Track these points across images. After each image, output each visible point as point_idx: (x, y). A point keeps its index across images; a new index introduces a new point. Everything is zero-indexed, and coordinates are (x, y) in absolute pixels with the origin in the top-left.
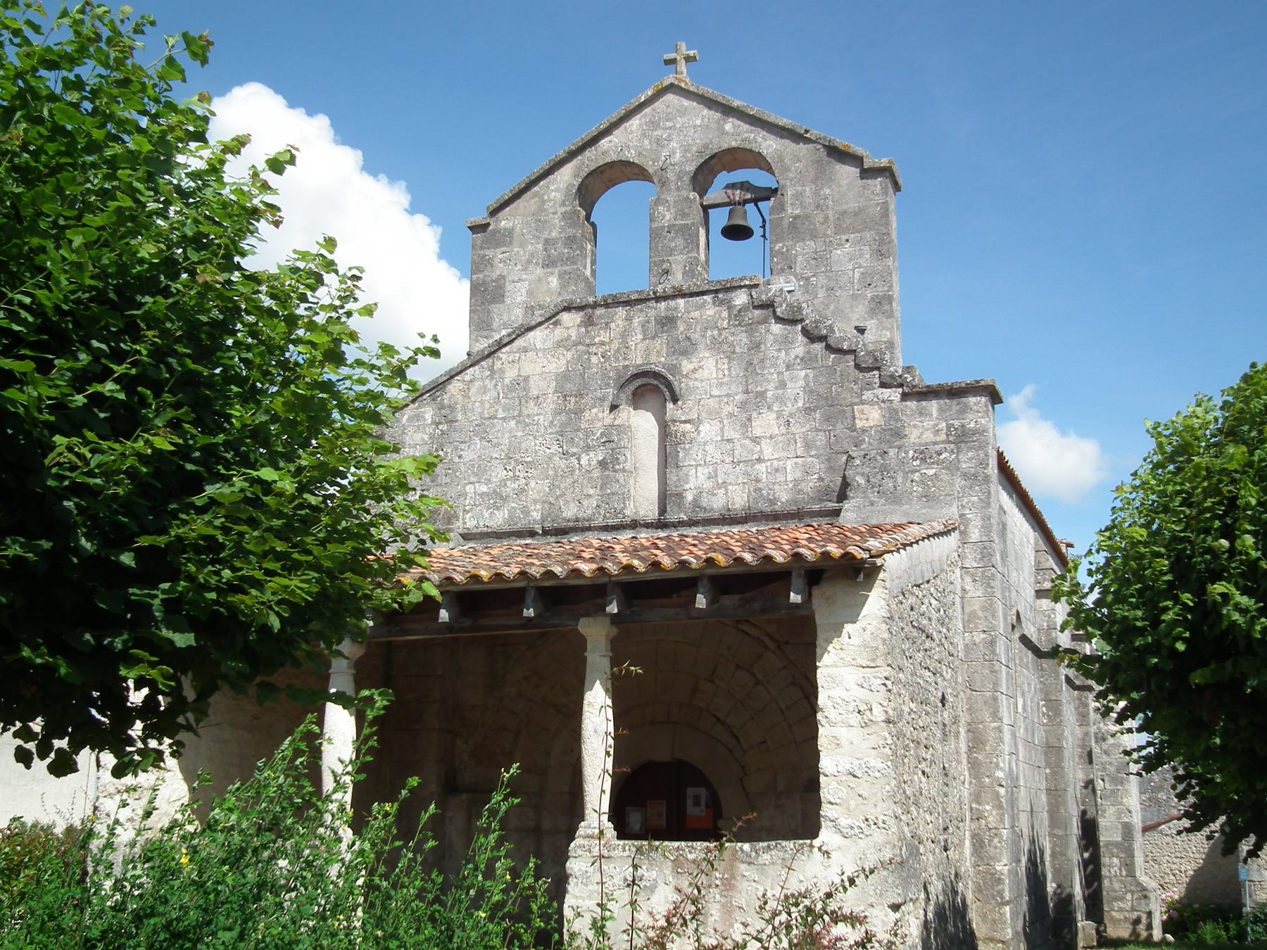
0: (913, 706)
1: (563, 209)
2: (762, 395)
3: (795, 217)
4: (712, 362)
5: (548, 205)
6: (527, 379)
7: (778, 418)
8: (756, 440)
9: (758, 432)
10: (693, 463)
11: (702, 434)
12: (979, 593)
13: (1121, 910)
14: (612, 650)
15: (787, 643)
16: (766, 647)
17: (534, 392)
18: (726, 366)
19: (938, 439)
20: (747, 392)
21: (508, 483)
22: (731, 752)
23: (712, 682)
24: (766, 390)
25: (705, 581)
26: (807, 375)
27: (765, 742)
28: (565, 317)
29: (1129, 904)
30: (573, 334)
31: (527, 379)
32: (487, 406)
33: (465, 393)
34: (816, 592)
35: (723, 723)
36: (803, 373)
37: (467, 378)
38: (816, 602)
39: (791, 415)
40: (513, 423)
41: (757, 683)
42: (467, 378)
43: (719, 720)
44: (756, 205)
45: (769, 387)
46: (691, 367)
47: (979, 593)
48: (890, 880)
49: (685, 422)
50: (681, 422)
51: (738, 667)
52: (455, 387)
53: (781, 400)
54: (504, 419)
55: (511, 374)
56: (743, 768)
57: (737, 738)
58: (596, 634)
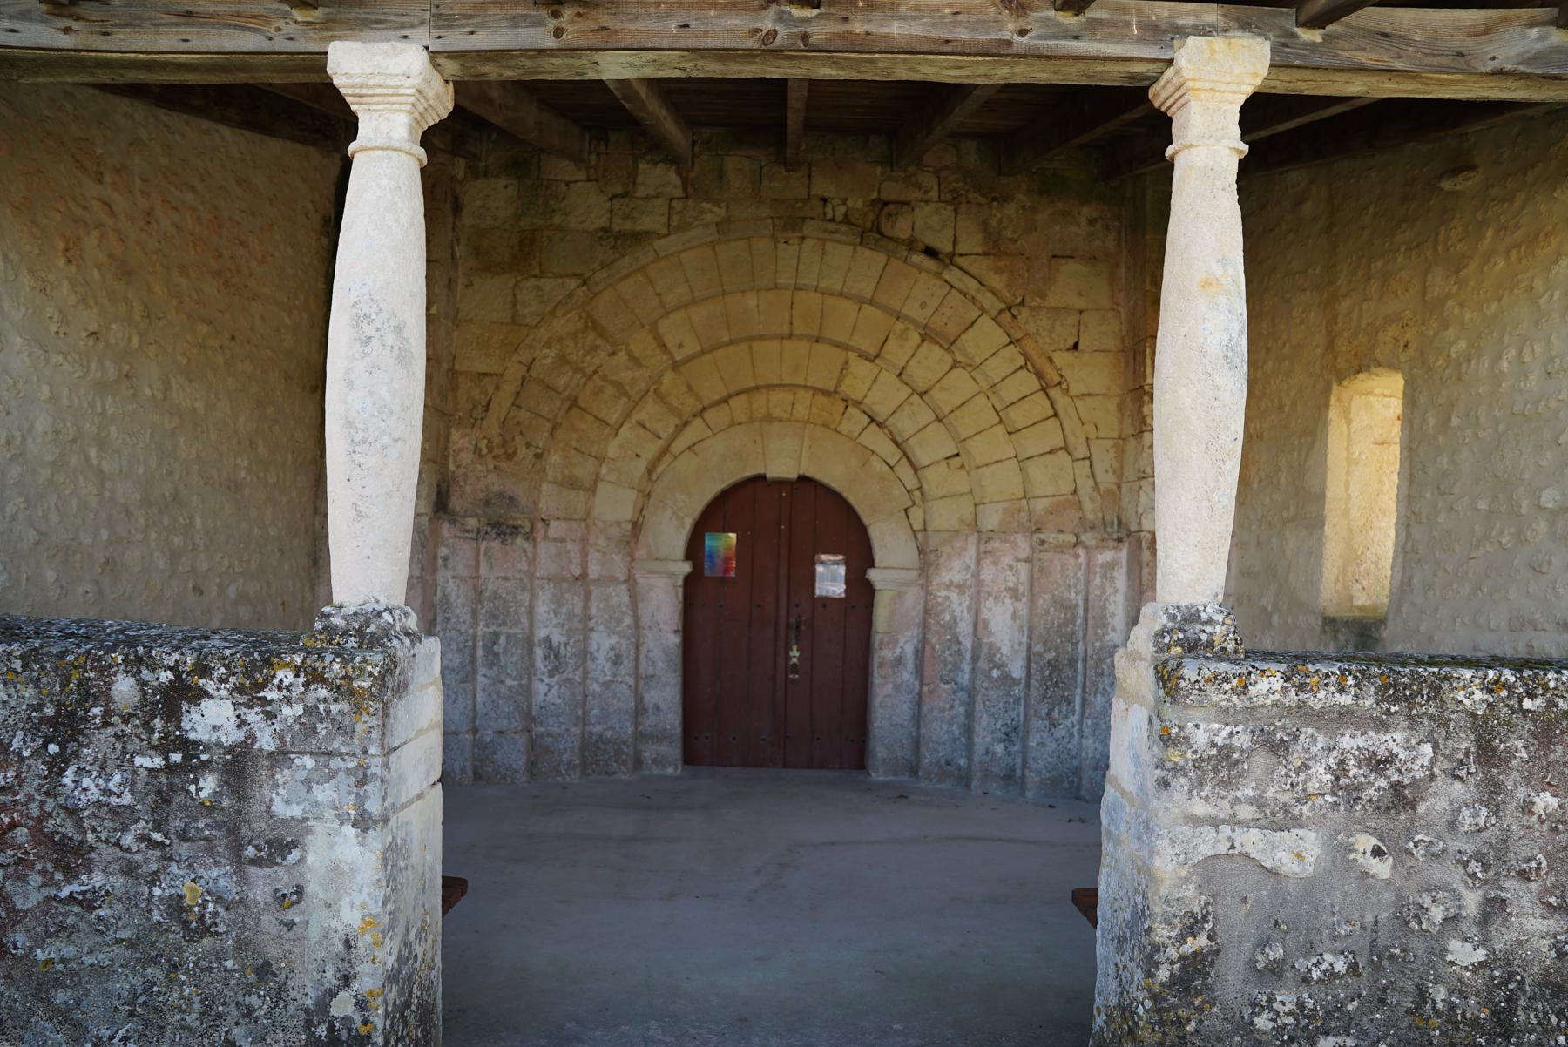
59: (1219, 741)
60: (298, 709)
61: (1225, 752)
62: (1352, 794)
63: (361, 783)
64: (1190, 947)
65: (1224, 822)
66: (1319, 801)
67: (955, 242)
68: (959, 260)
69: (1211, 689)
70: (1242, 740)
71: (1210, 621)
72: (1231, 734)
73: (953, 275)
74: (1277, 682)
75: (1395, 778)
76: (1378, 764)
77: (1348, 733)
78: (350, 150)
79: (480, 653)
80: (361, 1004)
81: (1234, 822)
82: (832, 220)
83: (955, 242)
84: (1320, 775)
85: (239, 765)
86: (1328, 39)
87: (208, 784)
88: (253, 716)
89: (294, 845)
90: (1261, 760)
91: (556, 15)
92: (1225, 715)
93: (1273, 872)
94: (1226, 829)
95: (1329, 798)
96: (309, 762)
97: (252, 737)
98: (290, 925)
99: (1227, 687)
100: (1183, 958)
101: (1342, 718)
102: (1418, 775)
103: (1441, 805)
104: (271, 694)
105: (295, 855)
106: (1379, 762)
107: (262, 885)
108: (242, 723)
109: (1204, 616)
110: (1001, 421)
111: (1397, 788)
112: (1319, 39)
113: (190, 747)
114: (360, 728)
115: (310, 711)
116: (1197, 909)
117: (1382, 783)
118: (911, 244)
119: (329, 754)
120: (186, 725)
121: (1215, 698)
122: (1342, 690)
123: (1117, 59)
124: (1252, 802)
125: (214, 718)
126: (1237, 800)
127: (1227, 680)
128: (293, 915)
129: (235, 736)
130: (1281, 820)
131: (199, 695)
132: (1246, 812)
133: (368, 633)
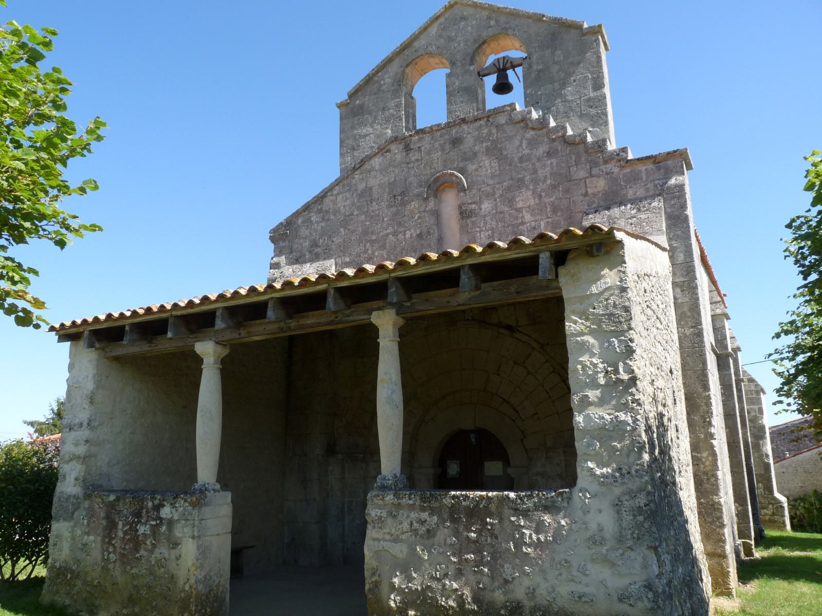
0: (652, 369)
1: (392, 88)
2: (521, 180)
3: (539, 71)
4: (487, 163)
5: (384, 88)
6: (371, 189)
7: (533, 193)
8: (519, 210)
9: (520, 205)
10: (478, 229)
11: (483, 210)
12: (687, 299)
13: (766, 514)
14: (400, 336)
15: (548, 344)
16: (533, 349)
17: (375, 196)
18: (497, 164)
19: (648, 194)
20: (512, 179)
21: (362, 255)
22: (514, 421)
23: (499, 375)
24: (524, 177)
25: (466, 269)
26: (552, 163)
27: (537, 413)
28: (393, 147)
29: (772, 511)
30: (398, 157)
31: (371, 189)
32: (348, 208)
33: (334, 202)
34: (561, 270)
35: (508, 402)
36: (549, 162)
37: (335, 192)
38: (562, 280)
39: (542, 190)
40: (363, 217)
41: (529, 373)
42: (335, 192)
43: (504, 400)
44: (514, 70)
45: (526, 174)
46: (474, 167)
47: (687, 299)
48: (646, 525)
49: (471, 204)
50: (469, 204)
51: (515, 363)
52: (327, 201)
53: (536, 181)
54: (357, 215)
55: (361, 186)
56: (523, 432)
57: (517, 412)
58: (386, 323)
59: (378, 514)
60: (182, 509)
61: (380, 518)
62: (415, 532)
63: (193, 527)
64: (374, 579)
65: (382, 540)
66: (406, 534)
67: (517, 321)
68: (520, 329)
69: (375, 499)
70: (384, 514)
71: (389, 480)
72: (381, 513)
73: (518, 335)
74: (392, 496)
75: (427, 527)
76: (423, 522)
77: (413, 513)
78: (202, 367)
79: (346, 509)
80: (191, 587)
81: (384, 540)
82: (468, 320)
83: (517, 321)
84: (406, 526)
85: (171, 523)
86: (411, 304)
87: (164, 528)
88: (174, 510)
89: (180, 544)
90: (390, 520)
91: (239, 330)
92: (379, 507)
93: (395, 556)
94: (381, 542)
95: (409, 533)
96: (183, 522)
97: (173, 516)
98: (178, 565)
99: (379, 498)
100: (372, 582)
101: (411, 508)
102: (434, 526)
103: (442, 537)
104: (177, 505)
105: (180, 546)
106: (422, 522)
107: (174, 553)
108: (171, 513)
109: (387, 478)
110: (550, 397)
111: (428, 531)
112: (409, 304)
113: (161, 519)
114: (194, 513)
115: (184, 509)
116: (375, 567)
117: (424, 529)
118: (500, 325)
119: (187, 520)
120: (161, 513)
121: (376, 502)
122: (410, 499)
123: (362, 320)
124: (389, 533)
125: (166, 512)
126: (384, 533)
127: (379, 496)
128: (178, 562)
129: (169, 516)
130: (396, 540)
131: (163, 506)
132: (388, 537)
133: (203, 491)
